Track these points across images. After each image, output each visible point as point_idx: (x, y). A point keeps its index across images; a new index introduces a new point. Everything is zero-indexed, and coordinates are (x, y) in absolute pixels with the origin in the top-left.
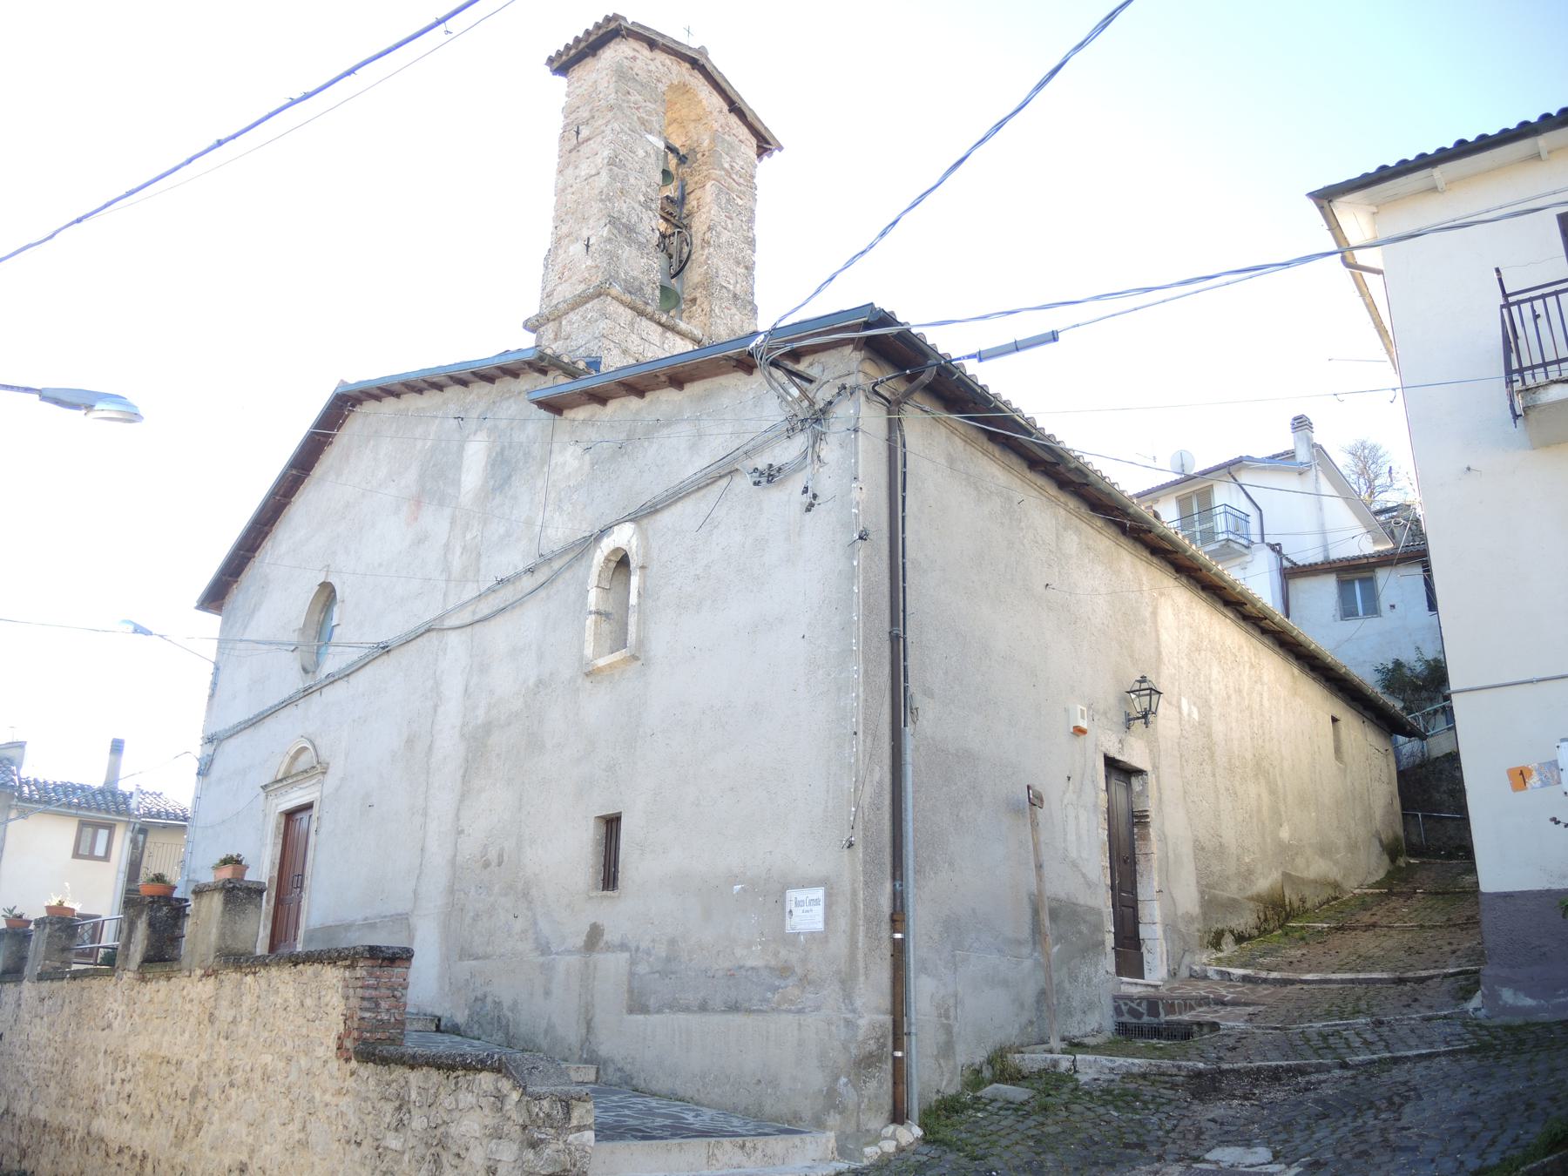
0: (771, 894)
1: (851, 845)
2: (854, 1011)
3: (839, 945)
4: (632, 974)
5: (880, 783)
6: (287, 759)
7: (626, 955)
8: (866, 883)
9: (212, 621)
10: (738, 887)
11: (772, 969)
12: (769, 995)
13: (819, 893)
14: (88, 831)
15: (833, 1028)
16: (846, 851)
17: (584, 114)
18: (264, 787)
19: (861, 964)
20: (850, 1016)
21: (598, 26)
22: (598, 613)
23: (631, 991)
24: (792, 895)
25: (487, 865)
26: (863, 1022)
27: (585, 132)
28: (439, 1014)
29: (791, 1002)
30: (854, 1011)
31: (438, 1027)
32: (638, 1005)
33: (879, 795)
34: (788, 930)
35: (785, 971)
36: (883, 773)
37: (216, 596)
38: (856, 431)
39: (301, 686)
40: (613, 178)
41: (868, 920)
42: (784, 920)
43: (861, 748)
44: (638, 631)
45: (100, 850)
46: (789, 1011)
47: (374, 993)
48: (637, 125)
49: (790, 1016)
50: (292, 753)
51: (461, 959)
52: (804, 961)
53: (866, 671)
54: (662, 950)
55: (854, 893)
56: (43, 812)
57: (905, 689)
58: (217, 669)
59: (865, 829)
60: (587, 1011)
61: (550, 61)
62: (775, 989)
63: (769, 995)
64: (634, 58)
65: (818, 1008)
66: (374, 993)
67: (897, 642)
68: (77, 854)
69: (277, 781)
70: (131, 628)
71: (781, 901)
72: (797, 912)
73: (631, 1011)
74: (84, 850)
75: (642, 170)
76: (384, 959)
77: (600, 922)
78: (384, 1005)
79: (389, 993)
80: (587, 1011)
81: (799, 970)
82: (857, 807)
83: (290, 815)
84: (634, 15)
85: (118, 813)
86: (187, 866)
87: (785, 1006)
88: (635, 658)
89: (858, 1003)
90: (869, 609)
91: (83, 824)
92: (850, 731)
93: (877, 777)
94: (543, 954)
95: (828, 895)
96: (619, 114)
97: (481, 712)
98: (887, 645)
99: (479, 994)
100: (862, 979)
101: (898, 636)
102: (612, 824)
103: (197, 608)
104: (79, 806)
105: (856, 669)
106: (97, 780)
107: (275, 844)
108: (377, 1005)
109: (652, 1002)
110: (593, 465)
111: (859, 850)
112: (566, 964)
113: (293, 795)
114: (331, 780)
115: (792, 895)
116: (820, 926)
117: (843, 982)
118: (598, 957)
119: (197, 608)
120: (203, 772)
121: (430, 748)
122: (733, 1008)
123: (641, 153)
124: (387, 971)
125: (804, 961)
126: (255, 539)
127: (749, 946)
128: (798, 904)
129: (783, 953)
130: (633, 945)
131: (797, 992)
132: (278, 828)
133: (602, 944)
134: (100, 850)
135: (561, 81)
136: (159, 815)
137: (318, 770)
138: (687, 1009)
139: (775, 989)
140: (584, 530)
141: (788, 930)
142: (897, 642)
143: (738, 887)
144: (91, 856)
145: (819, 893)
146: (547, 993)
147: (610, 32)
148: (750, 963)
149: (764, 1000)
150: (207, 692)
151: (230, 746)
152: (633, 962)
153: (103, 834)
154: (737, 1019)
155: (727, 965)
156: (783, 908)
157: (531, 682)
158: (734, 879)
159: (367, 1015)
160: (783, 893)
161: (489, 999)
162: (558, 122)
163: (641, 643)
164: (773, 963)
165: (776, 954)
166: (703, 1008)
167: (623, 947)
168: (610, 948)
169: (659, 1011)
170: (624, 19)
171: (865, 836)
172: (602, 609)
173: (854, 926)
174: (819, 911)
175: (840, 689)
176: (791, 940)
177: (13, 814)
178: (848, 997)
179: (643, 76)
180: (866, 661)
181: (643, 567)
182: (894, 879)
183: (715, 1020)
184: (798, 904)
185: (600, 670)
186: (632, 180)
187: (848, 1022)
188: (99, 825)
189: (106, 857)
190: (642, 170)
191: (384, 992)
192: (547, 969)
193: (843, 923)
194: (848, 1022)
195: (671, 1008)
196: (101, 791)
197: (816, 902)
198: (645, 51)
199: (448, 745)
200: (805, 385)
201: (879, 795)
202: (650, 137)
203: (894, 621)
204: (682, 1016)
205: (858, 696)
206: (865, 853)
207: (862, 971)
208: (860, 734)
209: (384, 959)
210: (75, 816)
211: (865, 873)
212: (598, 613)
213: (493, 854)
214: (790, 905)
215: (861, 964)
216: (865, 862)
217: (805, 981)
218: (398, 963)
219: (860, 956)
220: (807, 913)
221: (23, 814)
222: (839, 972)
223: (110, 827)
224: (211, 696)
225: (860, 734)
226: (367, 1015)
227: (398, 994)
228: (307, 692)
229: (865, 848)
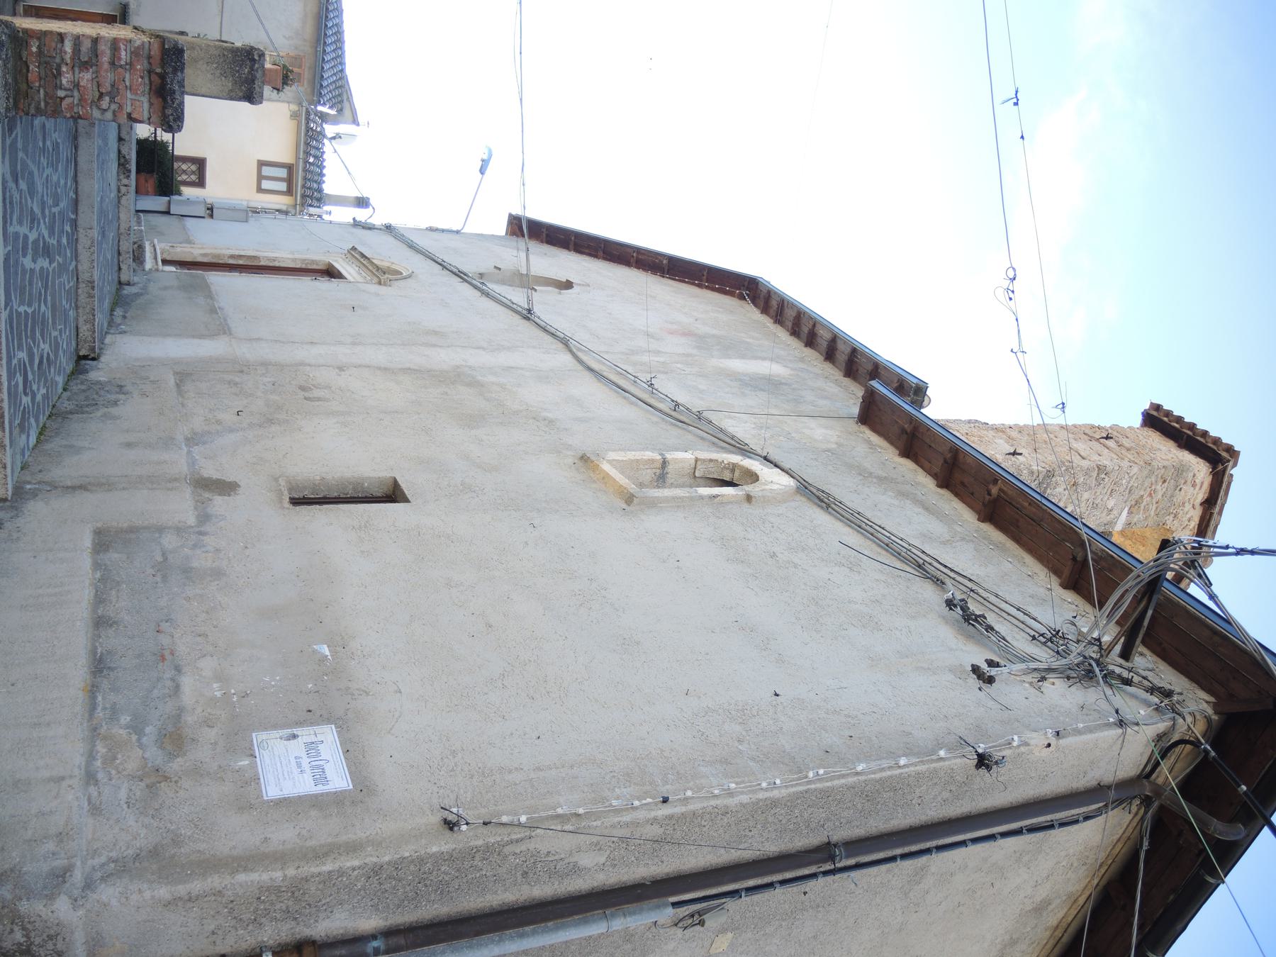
0: (322, 698)
1: (450, 825)
2: (89, 885)
3: (236, 834)
4: (161, 530)
5: (576, 870)
7: (192, 520)
8: (377, 870)
9: (501, 228)
10: (325, 650)
11: (178, 716)
12: (125, 719)
13: (339, 780)
14: (283, 173)
15: (50, 846)
16: (436, 819)
17: (1126, 442)
18: (354, 249)
19: (196, 886)
20: (78, 876)
21: (1217, 441)
22: (665, 463)
23: (133, 530)
24: (328, 736)
25: (303, 388)
26: (62, 909)
27: (1110, 443)
28: (102, 359)
29: (110, 760)
30: (89, 885)
31: (85, 357)
32: (103, 540)
33: (553, 873)
34: (257, 737)
35: (175, 739)
36: (597, 871)
38: (1121, 723)
40: (1087, 473)
41: (296, 889)
42: (275, 727)
43: (641, 815)
44: (667, 500)
45: (266, 185)
46: (91, 756)
47: (105, 59)
48: (1135, 496)
49: (79, 760)
51: (176, 373)
52: (197, 772)
53: (774, 803)
54: (201, 561)
55: (353, 848)
56: (298, 133)
57: (734, 894)
59: (488, 849)
60: (100, 485)
61: (1157, 407)
62: (137, 728)
63: (125, 719)
64: (1194, 485)
65: (95, 810)
66: (105, 59)
67: (826, 858)
68: (262, 164)
70: (485, 157)
71: (311, 717)
72: (297, 747)
73: (98, 533)
74: (267, 171)
75: (1095, 506)
76: (162, 77)
77: (240, 491)
78: (86, 77)
79: (106, 87)
80: (100, 485)
81: (177, 765)
82: (531, 827)
84: (1239, 474)
85: (303, 196)
87: (101, 749)
88: (630, 499)
89: (108, 893)
90: (869, 794)
91: (290, 168)
92: (665, 790)
93: (586, 860)
94: (187, 439)
95: (337, 800)
96: (1146, 472)
97: (491, 379)
98: (814, 840)
99: (129, 388)
100: (164, 892)
101: (832, 858)
102: (393, 495)
103: (510, 215)
104: (306, 162)
105: (775, 784)
106: (329, 187)
107: (294, 260)
108: (85, 66)
109: (113, 556)
110: (828, 450)
111: (444, 844)
112: (177, 461)
115: (328, 736)
116: (272, 791)
117: (155, 853)
118: (188, 492)
119: (510, 215)
121: (434, 346)
122: (99, 665)
123: (1111, 504)
124: (142, 84)
125: (197, 772)
126: (589, 247)
127: (220, 677)
128: (311, 747)
129: (211, 734)
130: (207, 528)
131: (132, 766)
132: (313, 262)
133: (207, 495)
134: (266, 185)
135: (1137, 421)
138: (99, 599)
139: (137, 728)
140: (754, 445)
141: (257, 737)
142: (826, 858)
143: (325, 650)
144: (260, 178)
145: (339, 780)
146: (129, 445)
147: (1218, 457)
148: (187, 682)
149: (114, 713)
152: (180, 530)
153: (283, 186)
154: (78, 673)
155: (182, 649)
156: (300, 724)
157: (550, 415)
158: (340, 643)
159: (68, 47)
160: (328, 721)
161: (122, 397)
162: (1106, 423)
163: (652, 504)
164: (189, 719)
165: (208, 723)
166: (100, 623)
167: (204, 518)
168: (201, 504)
169: (97, 566)
170: (1235, 465)
171: (472, 853)
172: (670, 468)
173: (280, 858)
174: (304, 785)
175: (725, 762)
176: (238, 741)
177: (294, 107)
178: (122, 868)
179: (1179, 497)
180: (791, 802)
181: (749, 498)
182: (389, 933)
183: (77, 642)
184: (311, 747)
185: (596, 468)
186: (1086, 495)
187: (60, 877)
188: (290, 181)
189: (260, 190)
190: (1095, 506)
191: (108, 77)
192: (168, 442)
193: (284, 835)
194: (60, 877)
195: (103, 580)
196: (320, 190)
197: (321, 777)
198: (1201, 495)
199: (443, 358)
200: (1118, 648)
201: (553, 873)
202: (1125, 513)
203: (857, 845)
204: (87, 594)
205: (731, 794)
206: (439, 858)
207: (182, 890)
208: (666, 810)
209: (162, 77)
210: (297, 158)
211: (397, 865)
212: (665, 463)
213: (316, 393)
214: (306, 735)
215: (196, 886)
216: (421, 861)
217: (154, 778)
218: (157, 102)
219: (215, 881)
220: (296, 765)
221: (294, 116)
222: (177, 841)
223: (289, 192)
225: (666, 810)
226: (68, 47)
227: (105, 103)
229: (450, 858)
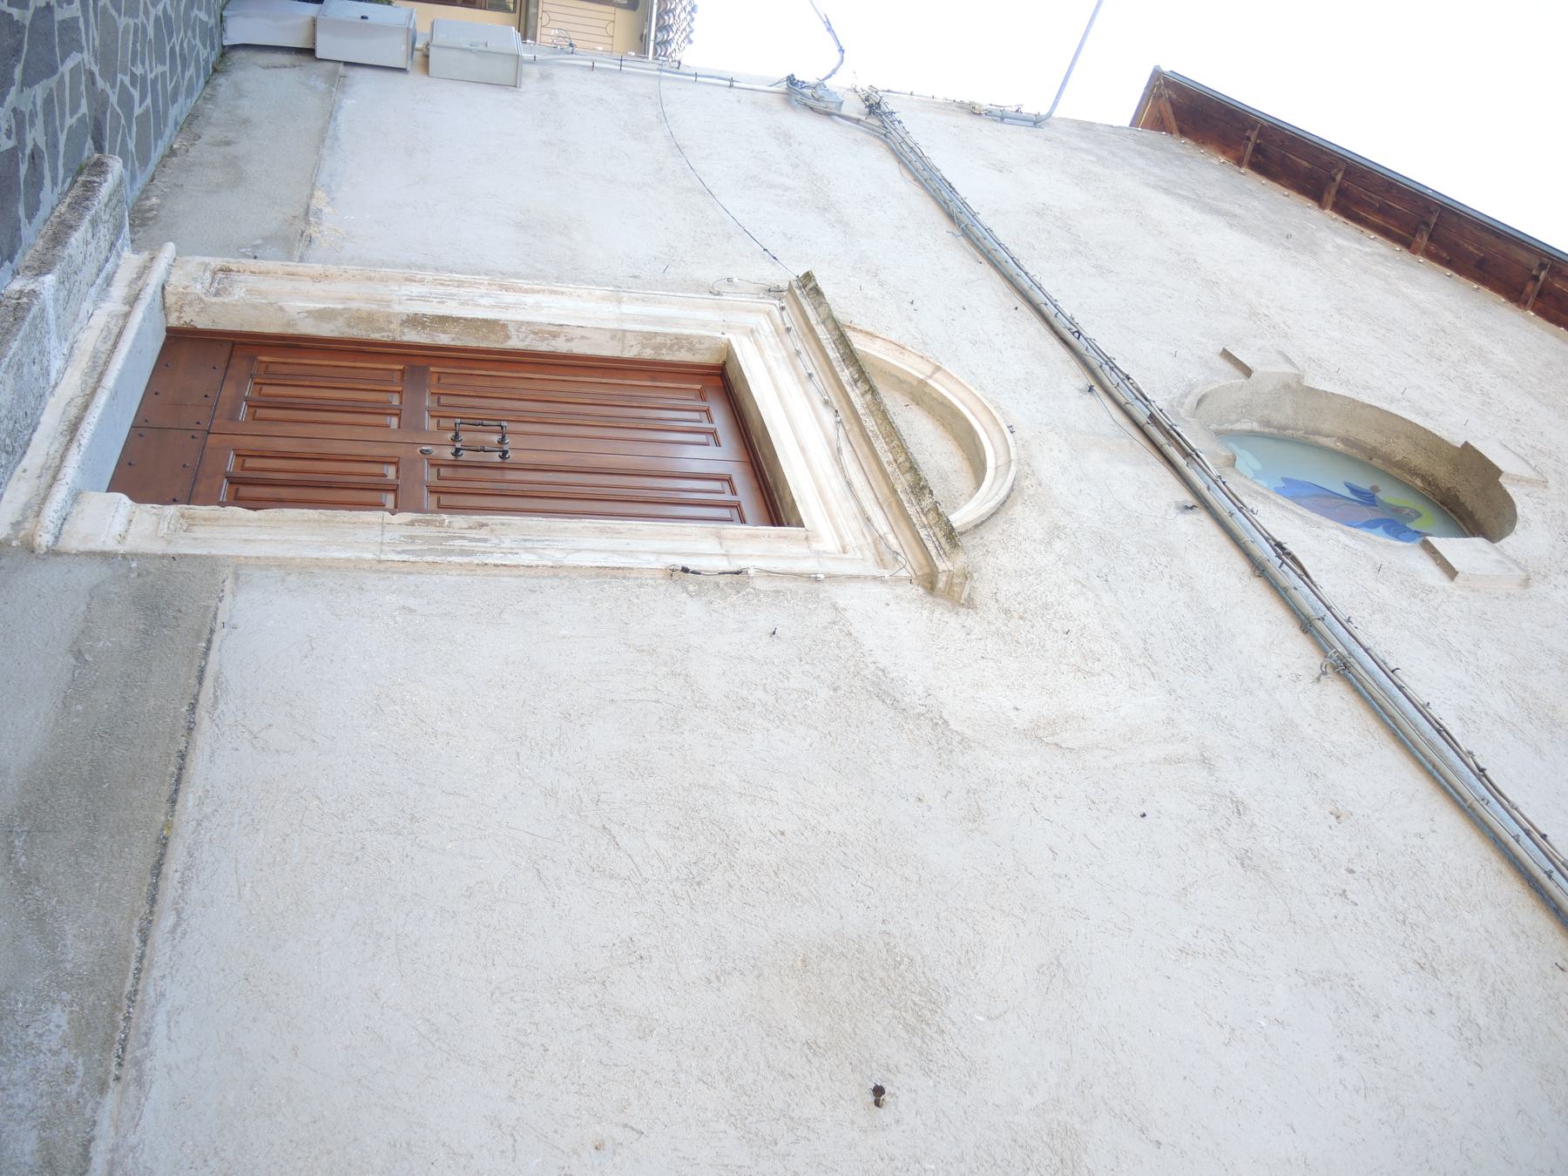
6: (914, 368)
9: (1119, 102)
37: (1190, 115)
39: (1160, 401)
50: (940, 386)
58: (1036, 122)
69: (843, 341)
83: (721, 381)
86: (970, 555)
107: (619, 335)
113: (786, 378)
114: (893, 625)
120: (796, 93)
132: (679, 341)
136: (663, 28)
137: (937, 555)
150: (984, 101)
151: (875, 161)
224: (973, 111)
228: (1158, 437)
